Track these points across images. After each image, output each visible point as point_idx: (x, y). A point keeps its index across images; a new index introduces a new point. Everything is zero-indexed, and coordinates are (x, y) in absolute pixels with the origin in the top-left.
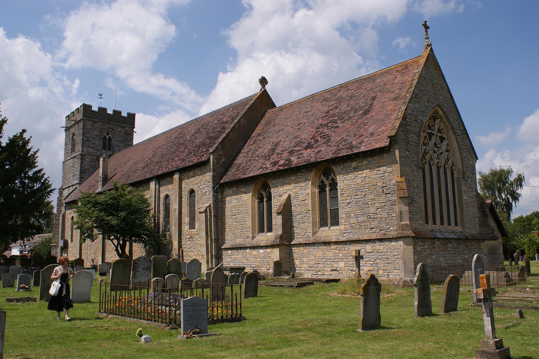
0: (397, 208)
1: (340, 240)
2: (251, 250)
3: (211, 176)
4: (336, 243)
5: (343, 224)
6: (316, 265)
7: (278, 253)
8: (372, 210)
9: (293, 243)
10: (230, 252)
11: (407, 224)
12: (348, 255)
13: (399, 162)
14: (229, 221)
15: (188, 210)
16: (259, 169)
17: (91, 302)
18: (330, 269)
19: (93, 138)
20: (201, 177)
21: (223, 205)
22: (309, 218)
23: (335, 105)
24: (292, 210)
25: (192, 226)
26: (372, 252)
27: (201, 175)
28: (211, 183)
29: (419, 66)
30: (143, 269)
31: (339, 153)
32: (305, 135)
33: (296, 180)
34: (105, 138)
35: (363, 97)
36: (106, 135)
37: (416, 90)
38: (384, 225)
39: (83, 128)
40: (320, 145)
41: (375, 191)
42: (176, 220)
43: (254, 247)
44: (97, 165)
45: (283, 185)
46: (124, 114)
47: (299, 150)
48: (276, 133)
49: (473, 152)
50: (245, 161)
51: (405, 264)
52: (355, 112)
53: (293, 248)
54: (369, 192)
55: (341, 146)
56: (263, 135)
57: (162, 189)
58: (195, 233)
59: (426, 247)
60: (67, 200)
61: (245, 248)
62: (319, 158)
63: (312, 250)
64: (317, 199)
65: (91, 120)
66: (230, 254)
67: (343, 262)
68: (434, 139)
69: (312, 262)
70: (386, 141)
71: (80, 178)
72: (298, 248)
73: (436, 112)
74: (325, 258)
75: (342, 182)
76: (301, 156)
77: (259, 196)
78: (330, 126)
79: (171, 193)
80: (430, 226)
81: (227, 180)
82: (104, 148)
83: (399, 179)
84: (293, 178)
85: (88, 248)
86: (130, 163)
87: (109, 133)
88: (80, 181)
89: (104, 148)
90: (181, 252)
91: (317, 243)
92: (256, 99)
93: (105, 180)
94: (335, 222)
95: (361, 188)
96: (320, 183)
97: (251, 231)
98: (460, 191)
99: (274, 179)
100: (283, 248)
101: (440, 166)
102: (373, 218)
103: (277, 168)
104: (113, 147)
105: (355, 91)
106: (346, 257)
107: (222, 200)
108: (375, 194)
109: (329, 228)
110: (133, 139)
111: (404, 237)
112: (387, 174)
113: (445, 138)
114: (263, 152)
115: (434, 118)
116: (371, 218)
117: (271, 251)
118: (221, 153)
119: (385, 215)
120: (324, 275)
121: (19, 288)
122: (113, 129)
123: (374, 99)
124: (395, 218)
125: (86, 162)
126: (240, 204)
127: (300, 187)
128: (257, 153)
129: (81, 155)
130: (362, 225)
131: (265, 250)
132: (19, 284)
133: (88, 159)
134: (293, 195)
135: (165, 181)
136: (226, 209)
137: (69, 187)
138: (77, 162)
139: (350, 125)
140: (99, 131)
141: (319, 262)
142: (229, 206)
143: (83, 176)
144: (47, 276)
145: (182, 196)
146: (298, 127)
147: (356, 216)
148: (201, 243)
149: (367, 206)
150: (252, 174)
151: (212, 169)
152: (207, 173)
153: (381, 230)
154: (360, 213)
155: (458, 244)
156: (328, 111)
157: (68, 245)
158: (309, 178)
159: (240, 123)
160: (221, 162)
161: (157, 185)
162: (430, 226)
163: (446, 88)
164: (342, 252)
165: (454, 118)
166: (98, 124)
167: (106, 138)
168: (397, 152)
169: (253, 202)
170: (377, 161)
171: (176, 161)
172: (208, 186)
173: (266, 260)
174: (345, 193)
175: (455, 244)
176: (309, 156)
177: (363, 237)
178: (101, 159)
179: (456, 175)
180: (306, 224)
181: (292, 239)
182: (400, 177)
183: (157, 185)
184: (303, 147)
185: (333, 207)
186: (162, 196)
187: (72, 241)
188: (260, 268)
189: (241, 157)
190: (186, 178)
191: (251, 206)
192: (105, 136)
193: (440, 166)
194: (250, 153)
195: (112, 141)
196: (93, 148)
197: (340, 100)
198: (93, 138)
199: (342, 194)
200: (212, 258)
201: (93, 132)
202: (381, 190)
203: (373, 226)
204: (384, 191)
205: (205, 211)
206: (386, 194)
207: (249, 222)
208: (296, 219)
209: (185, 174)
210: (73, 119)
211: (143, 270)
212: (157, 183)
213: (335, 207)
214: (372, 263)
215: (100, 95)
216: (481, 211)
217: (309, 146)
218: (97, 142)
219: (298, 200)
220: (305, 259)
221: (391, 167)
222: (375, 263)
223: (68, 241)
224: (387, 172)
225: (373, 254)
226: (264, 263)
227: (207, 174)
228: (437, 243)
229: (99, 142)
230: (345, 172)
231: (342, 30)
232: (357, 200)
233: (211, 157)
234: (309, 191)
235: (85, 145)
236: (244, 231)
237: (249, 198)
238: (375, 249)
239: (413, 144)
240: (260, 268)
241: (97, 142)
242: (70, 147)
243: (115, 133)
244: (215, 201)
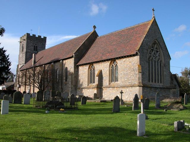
28: (73, 65)
34: (35, 46)
46: (42, 37)
59: (148, 90)
60: (20, 70)
68: (154, 51)
73: (155, 42)
80: (151, 83)
82: (34, 50)
89: (34, 50)
93: (35, 62)
98: (163, 71)
115: (155, 43)
119: (134, 78)
133: (28, 54)
138: (24, 55)
162: (151, 83)
163: (160, 33)
175: (159, 90)
178: (33, 54)
179: (162, 65)
186: (97, 73)
196: (30, 50)
202: (133, 70)
212: (64, 64)
228: (152, 89)
229: (33, 48)
233: (74, 54)
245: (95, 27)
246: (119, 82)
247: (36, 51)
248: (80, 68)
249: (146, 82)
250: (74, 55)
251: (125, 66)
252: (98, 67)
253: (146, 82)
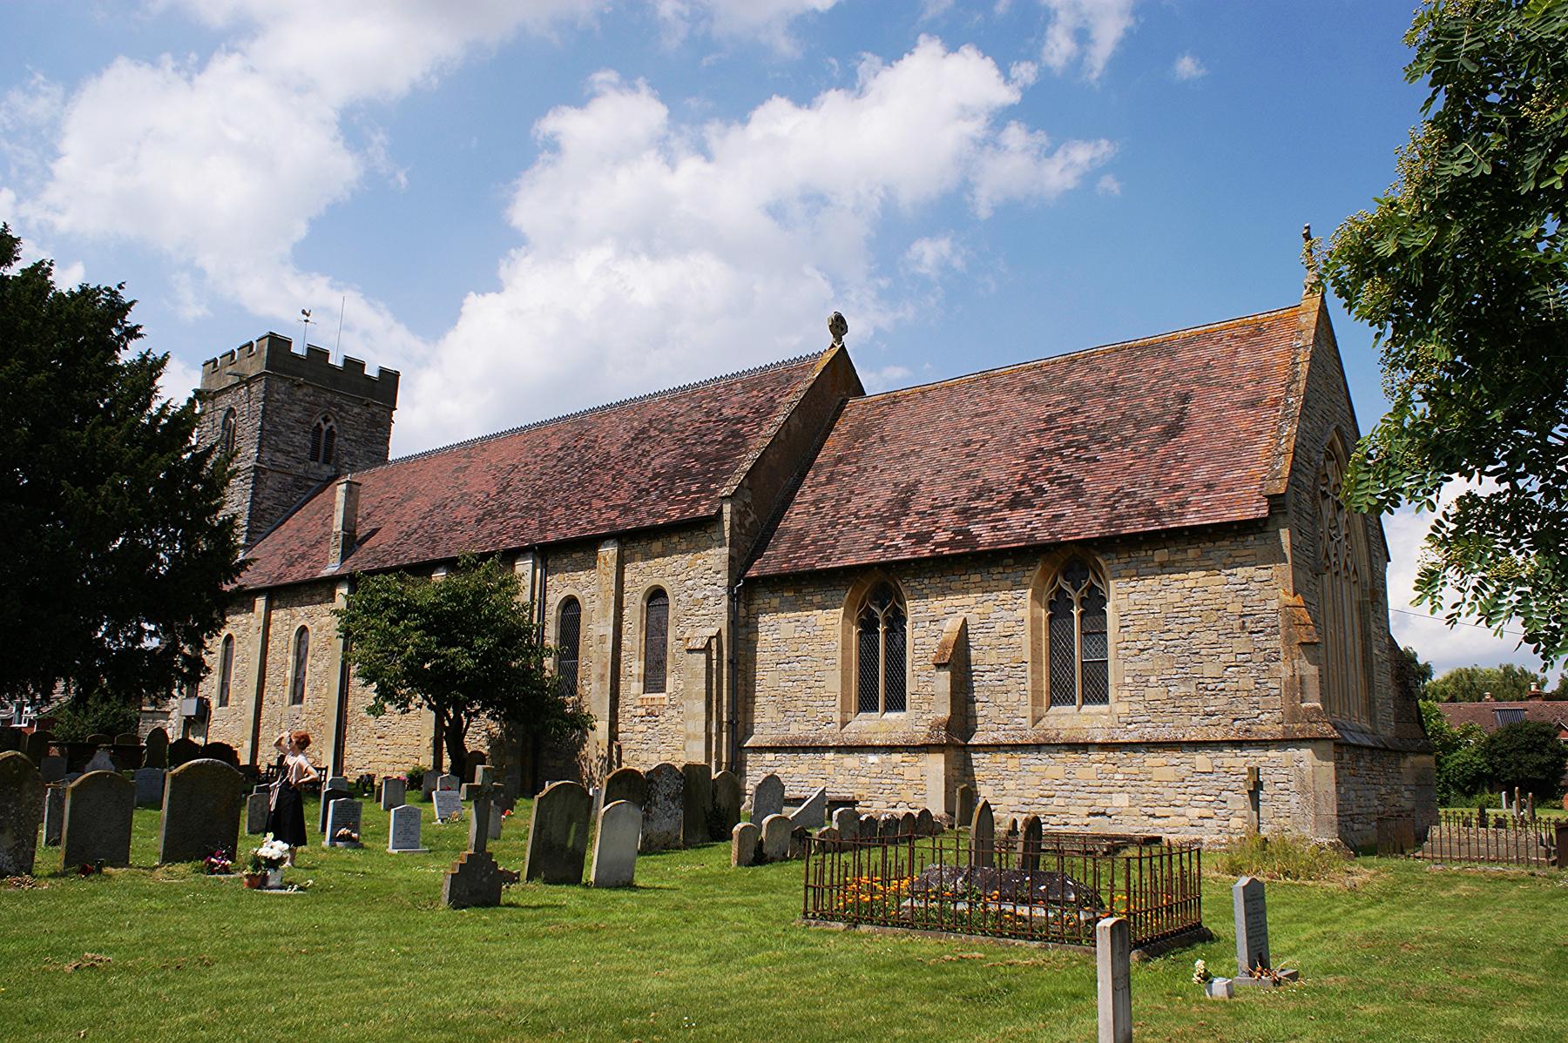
0: (1284, 670)
1: (1120, 741)
2: (840, 755)
3: (725, 558)
4: (1104, 746)
5: (1125, 699)
6: (1045, 801)
7: (942, 767)
8: (1210, 670)
9: (974, 741)
10: (770, 756)
11: (1316, 708)
12: (1141, 777)
13: (1289, 558)
15: (641, 640)
16: (871, 549)
17: (635, 886)
18: (1086, 810)
19: (288, 427)
20: (689, 557)
21: (750, 636)
22: (1024, 680)
23: (1068, 405)
24: (972, 658)
25: (654, 679)
26: (1212, 773)
27: (689, 552)
28: (724, 574)
29: (1302, 331)
31: (1122, 525)
32: (999, 471)
33: (986, 584)
35: (1150, 390)
36: (322, 422)
38: (1244, 707)
39: (264, 399)
40: (1052, 500)
41: (1221, 623)
42: (605, 666)
43: (850, 747)
44: (294, 499)
45: (943, 593)
47: (991, 510)
48: (898, 460)
50: (815, 526)
52: (1138, 425)
53: (973, 755)
54: (1201, 625)
55: (1121, 508)
56: (856, 463)
57: (553, 580)
58: (666, 702)
61: (826, 749)
62: (1061, 532)
63: (1032, 761)
64: (1044, 635)
65: (287, 379)
66: (769, 764)
67: (1127, 795)
69: (1033, 791)
70: (1258, 505)
71: (247, 531)
72: (988, 756)
74: (1071, 782)
75: (1126, 596)
76: (1000, 525)
77: (863, 617)
78: (1068, 456)
79: (583, 593)
81: (769, 571)
82: (314, 457)
83: (1291, 600)
84: (976, 578)
85: (283, 725)
86: (421, 504)
87: (330, 417)
89: (314, 457)
90: (615, 750)
91: (1052, 744)
92: (825, 368)
93: (350, 543)
94: (1097, 692)
95: (1181, 615)
96: (1053, 596)
97: (838, 706)
99: (916, 576)
100: (953, 753)
102: (1212, 690)
103: (932, 551)
104: (338, 455)
105: (1120, 373)
106: (1133, 783)
107: (748, 622)
108: (1220, 632)
109: (1079, 709)
110: (388, 439)
111: (1316, 740)
112: (1254, 584)
114: (869, 506)
116: (1207, 689)
117: (905, 759)
118: (748, 500)
120: (1066, 824)
121: (334, 839)
122: (341, 409)
123: (1185, 398)
124: (1277, 692)
125: (267, 491)
126: (803, 634)
127: (997, 603)
128: (852, 507)
129: (256, 469)
130: (1182, 704)
131: (884, 756)
132: (333, 828)
133: (271, 482)
134: (974, 621)
135: (565, 560)
136: (759, 645)
139: (1133, 458)
140: (305, 409)
141: (1052, 793)
142: (770, 638)
143: (257, 527)
144: (549, 814)
145: (622, 603)
146: (966, 450)
147: (1165, 683)
148: (690, 731)
149: (1196, 659)
150: (851, 561)
151: (728, 540)
152: (710, 548)
153: (1235, 720)
154: (1176, 676)
156: (1050, 419)
157: (210, 712)
158: (1026, 580)
159: (789, 426)
161: (538, 571)
163: (1343, 390)
166: (305, 390)
167: (321, 430)
168: (1285, 535)
169: (846, 631)
170: (1228, 552)
171: (599, 510)
172: (714, 581)
173: (888, 781)
174: (1131, 623)
176: (1021, 524)
177: (1187, 735)
180: (1013, 697)
181: (971, 731)
182: (1292, 593)
183: (538, 571)
184: (999, 502)
185: (1091, 657)
187: (224, 702)
188: (869, 803)
189: (797, 514)
190: (638, 556)
191: (840, 641)
192: (319, 424)
194: (827, 505)
195: (336, 439)
196: (287, 453)
197: (1080, 394)
198: (288, 427)
199: (1123, 627)
201: (291, 411)
202: (1237, 624)
203: (1213, 708)
204: (1247, 625)
205: (708, 647)
206: (1251, 633)
207: (833, 683)
209: (639, 547)
211: (666, 800)
212: (539, 565)
213: (1096, 657)
214: (1212, 798)
215: (304, 312)
216: (1398, 685)
217: (1016, 502)
218: (297, 439)
219: (990, 635)
220: (1010, 785)
221: (1267, 569)
222: (1220, 798)
223: (208, 703)
224: (1256, 579)
225: (1214, 777)
226: (881, 791)
227: (709, 552)
229: (302, 440)
230: (1134, 572)
231: (776, 211)
232: (1168, 643)
233: (727, 508)
234: (1025, 613)
235: (265, 443)
236: (816, 704)
237: (836, 621)
238: (1219, 765)
240: (869, 803)
241: (297, 439)
243: (344, 418)
244: (733, 622)
247: (326, 468)
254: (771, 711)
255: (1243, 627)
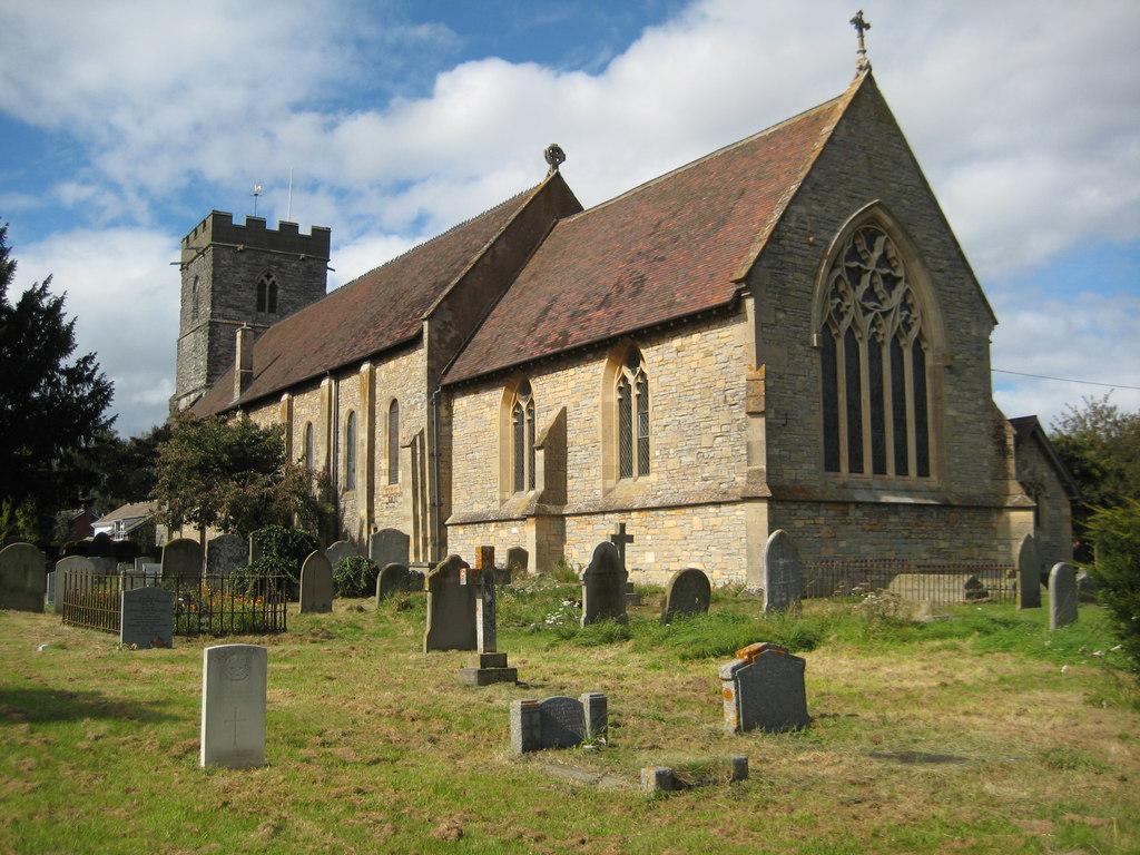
4: (640, 510)
14: (459, 467)
28: (425, 384)
30: (229, 560)
34: (262, 286)
37: (816, 175)
49: (983, 308)
51: (749, 555)
59: (821, 520)
68: (866, 280)
73: (875, 220)
81: (456, 378)
83: (753, 374)
88: (208, 381)
93: (246, 381)
101: (883, 342)
113: (901, 278)
119: (727, 451)
137: (190, 393)
138: (203, 337)
155: (919, 516)
159: (495, 252)
160: (448, 339)
164: (652, 531)
165: (931, 232)
167: (265, 286)
179: (929, 362)
180: (593, 472)
181: (563, 501)
186: (544, 423)
193: (883, 342)
198: (235, 286)
200: (425, 545)
202: (721, 398)
205: (413, 444)
207: (496, 469)
208: (575, 457)
210: (194, 244)
228: (854, 513)
229: (250, 295)
239: (799, 294)
242: (190, 306)
245: (555, 155)
246: (653, 477)
248: (462, 404)
249: (807, 471)
250: (426, 329)
251: (684, 379)
252: (553, 392)
253: (807, 471)
254: (464, 495)
255: (725, 401)
